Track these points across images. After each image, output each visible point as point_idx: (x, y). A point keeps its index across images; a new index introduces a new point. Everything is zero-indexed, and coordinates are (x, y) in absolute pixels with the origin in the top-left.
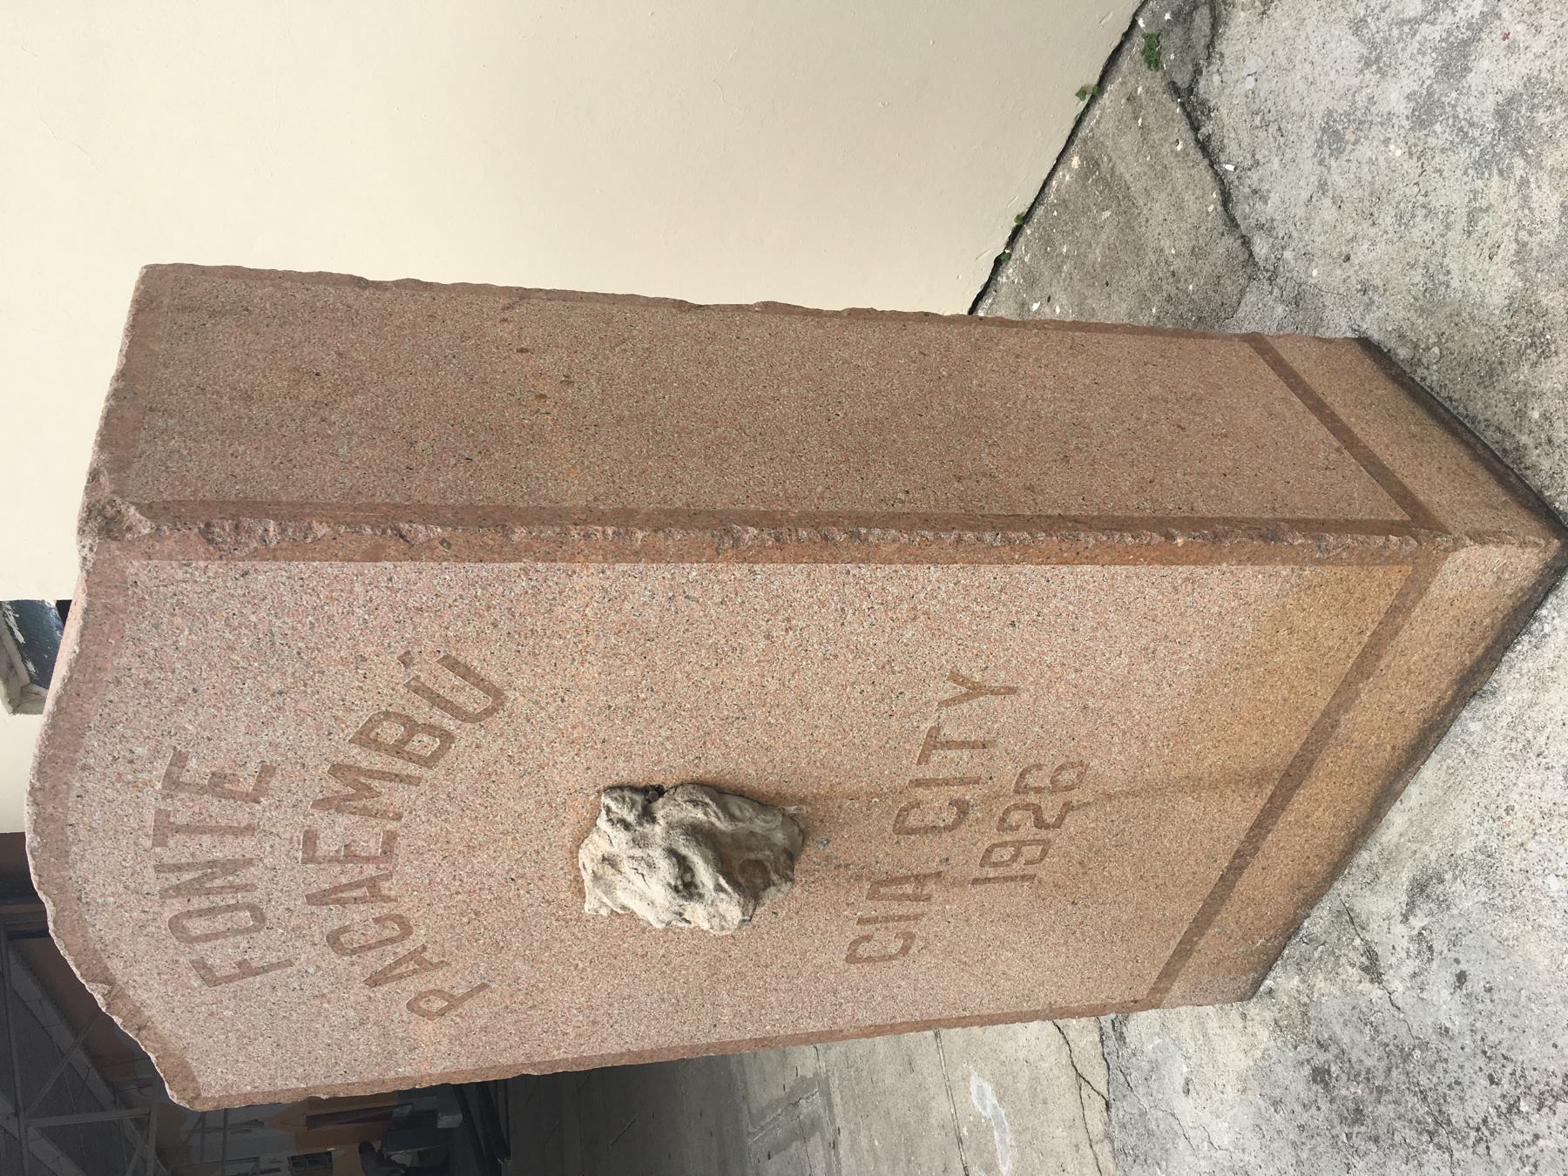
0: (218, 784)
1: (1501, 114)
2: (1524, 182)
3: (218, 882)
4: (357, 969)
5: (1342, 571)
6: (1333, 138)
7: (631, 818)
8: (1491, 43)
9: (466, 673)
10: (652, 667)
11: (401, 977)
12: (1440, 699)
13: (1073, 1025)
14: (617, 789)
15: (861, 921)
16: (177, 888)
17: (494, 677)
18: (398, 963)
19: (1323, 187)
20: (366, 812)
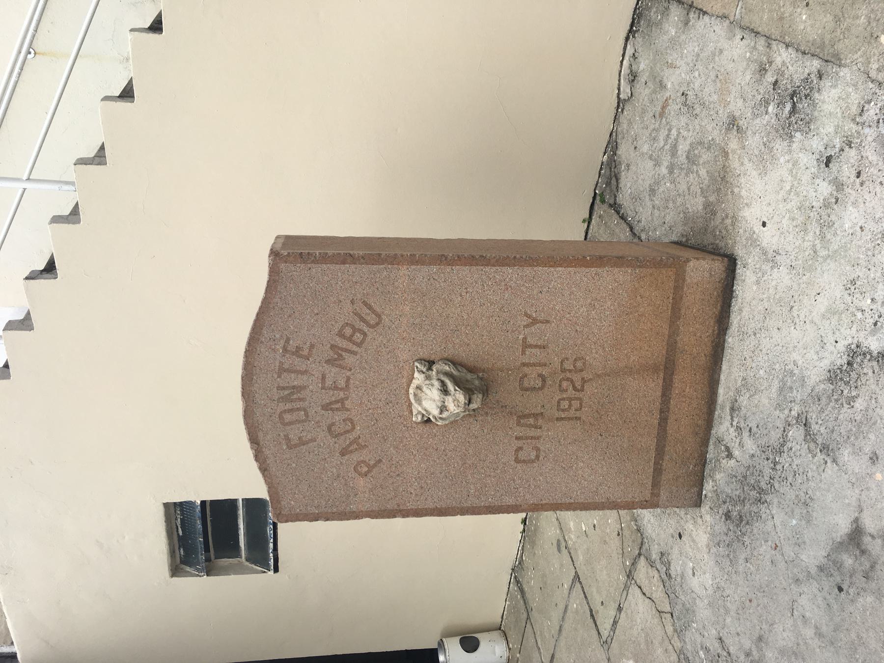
0: (297, 352)
1: (687, 157)
2: (697, 171)
3: (295, 396)
4: (337, 445)
5: (650, 271)
6: (652, 191)
7: (424, 370)
8: (681, 140)
9: (370, 308)
10: (425, 307)
11: (351, 452)
12: (714, 331)
13: (622, 512)
14: (420, 360)
15: (517, 438)
16: (282, 398)
17: (378, 310)
18: (351, 444)
19: (654, 207)
20: (341, 367)
